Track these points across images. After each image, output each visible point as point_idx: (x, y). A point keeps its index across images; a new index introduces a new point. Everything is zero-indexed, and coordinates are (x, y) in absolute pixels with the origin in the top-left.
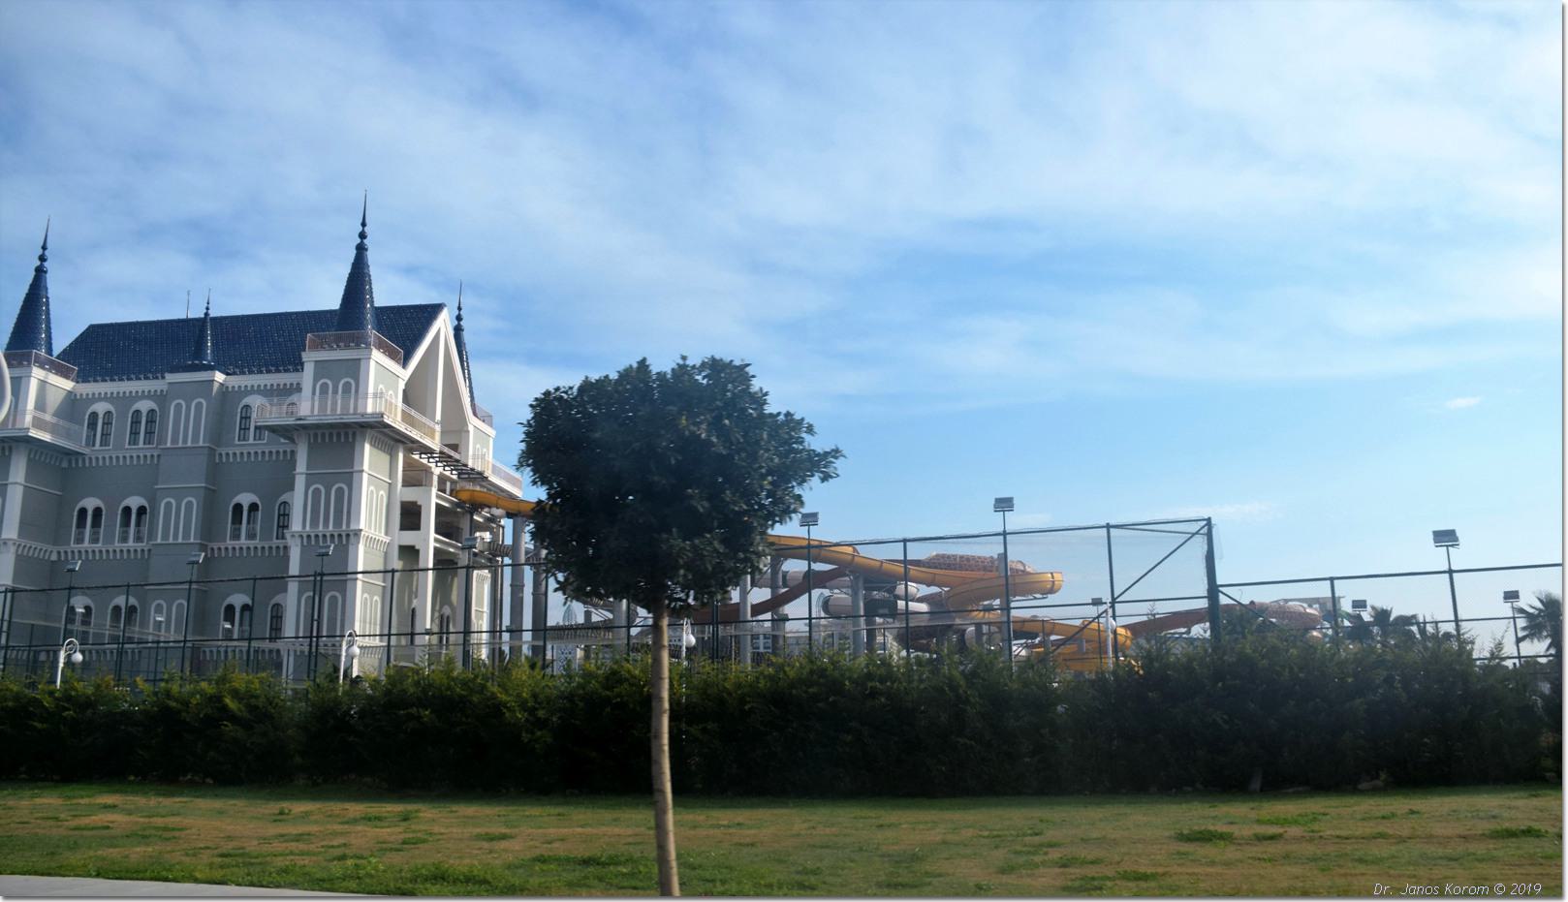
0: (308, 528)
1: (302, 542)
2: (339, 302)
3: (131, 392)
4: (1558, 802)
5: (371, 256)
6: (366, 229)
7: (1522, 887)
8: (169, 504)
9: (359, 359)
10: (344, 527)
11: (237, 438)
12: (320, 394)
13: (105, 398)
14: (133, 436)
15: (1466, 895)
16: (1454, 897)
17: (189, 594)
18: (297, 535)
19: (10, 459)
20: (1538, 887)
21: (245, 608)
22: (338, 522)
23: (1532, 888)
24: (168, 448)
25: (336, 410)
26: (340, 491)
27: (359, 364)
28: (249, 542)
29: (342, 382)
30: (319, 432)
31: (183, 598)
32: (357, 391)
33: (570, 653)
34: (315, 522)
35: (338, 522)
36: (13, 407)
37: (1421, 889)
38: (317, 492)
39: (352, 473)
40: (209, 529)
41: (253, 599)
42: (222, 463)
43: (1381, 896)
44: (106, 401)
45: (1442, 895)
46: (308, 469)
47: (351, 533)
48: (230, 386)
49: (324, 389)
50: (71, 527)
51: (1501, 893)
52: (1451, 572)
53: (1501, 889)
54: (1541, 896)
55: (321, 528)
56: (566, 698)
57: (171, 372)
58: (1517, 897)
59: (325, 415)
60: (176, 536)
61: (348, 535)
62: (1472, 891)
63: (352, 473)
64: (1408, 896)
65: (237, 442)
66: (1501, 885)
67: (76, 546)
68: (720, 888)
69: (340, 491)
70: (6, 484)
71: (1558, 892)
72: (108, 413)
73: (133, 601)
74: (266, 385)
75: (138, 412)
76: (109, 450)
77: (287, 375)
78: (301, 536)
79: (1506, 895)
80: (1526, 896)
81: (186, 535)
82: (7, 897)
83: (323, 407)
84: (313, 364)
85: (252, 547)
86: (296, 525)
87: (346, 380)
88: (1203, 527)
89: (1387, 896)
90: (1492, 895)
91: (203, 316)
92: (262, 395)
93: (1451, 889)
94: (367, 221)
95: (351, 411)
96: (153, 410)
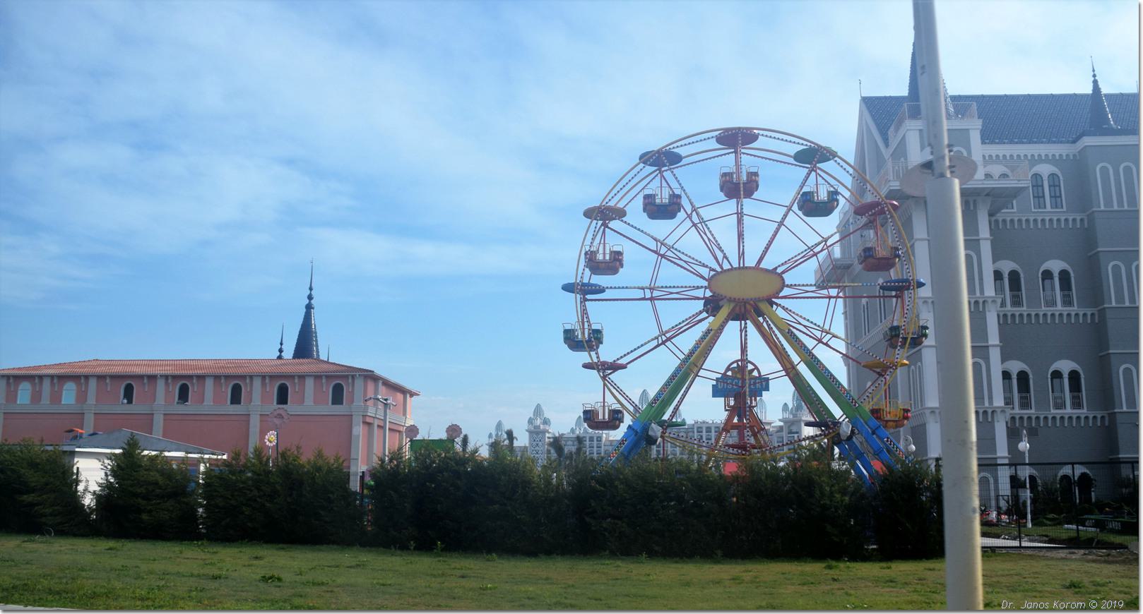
4: (1134, 537)
7: (1110, 604)
9: (968, 130)
14: (1041, 195)
15: (1069, 609)
16: (1059, 610)
19: (976, 212)
20: (1121, 603)
23: (1117, 604)
28: (1015, 309)
29: (1122, 167)
35: (922, 406)
37: (1036, 605)
39: (979, 240)
42: (1015, 229)
43: (1007, 610)
45: (1019, 609)
51: (1094, 607)
54: (1123, 609)
58: (1106, 610)
62: (1073, 606)
63: (979, 240)
64: (1026, 610)
65: (1033, 210)
66: (1094, 602)
68: (333, 606)
71: (1133, 604)
72: (1052, 175)
75: (1036, 176)
76: (1014, 213)
79: (1099, 609)
80: (1112, 609)
85: (1017, 314)
87: (1101, 165)
88: (785, 297)
89: (1011, 610)
90: (1087, 609)
91: (1088, 89)
96: (1053, 174)
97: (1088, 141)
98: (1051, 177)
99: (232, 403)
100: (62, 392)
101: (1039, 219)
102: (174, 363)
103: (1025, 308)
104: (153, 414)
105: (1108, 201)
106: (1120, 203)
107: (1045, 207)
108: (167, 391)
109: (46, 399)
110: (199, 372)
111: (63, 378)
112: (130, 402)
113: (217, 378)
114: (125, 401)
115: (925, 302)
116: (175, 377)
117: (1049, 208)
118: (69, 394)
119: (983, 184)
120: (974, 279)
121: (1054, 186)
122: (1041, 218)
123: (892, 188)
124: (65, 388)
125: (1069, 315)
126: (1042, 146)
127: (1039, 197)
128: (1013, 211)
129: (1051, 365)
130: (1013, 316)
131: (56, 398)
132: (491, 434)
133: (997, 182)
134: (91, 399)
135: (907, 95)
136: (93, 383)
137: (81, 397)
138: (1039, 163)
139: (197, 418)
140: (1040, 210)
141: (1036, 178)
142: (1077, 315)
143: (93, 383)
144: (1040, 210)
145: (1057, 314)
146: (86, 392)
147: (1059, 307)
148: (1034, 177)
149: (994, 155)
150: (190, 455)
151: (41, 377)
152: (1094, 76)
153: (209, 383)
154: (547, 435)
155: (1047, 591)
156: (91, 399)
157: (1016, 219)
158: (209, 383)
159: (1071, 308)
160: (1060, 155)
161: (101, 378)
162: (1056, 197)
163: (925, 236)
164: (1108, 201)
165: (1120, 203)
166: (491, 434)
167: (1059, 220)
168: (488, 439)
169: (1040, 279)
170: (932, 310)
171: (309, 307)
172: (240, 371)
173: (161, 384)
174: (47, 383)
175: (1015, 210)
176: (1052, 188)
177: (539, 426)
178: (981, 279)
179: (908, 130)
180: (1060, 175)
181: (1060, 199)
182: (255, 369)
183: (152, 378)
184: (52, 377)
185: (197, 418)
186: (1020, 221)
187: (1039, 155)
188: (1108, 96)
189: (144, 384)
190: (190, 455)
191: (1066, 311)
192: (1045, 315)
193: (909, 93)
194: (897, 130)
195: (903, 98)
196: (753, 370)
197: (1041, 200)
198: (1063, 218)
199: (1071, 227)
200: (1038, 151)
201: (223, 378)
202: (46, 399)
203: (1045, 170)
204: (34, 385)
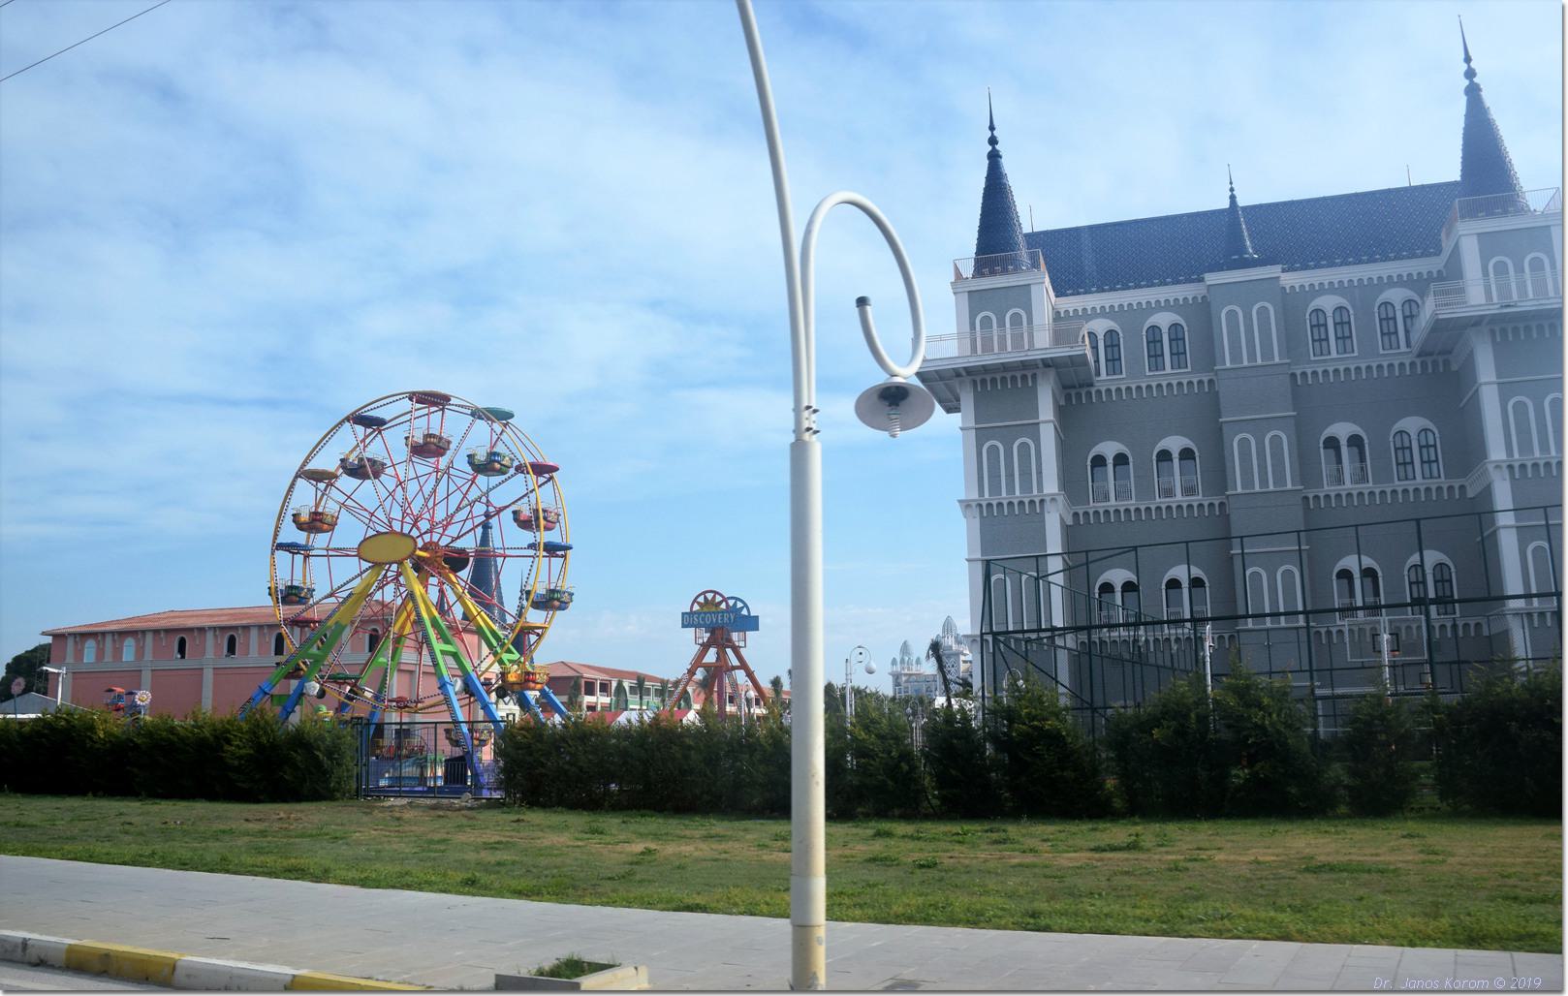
0: (987, 496)
1: (981, 512)
2: (1459, 167)
3: (1331, 283)
5: (1007, 164)
6: (1472, 65)
8: (1244, 443)
10: (1035, 492)
11: (1381, 348)
12: (1011, 325)
13: (1167, 306)
14: (1159, 353)
17: (1300, 554)
18: (974, 504)
20: (1538, 981)
21: (1129, 587)
22: (1026, 486)
23: (1532, 981)
24: (1277, 365)
25: (1526, 293)
26: (1024, 447)
27: (1550, 233)
30: (1008, 375)
31: (1542, 539)
32: (1030, 321)
33: (953, 666)
34: (995, 489)
35: (1026, 486)
36: (1560, 279)
38: (993, 450)
40: (1306, 471)
41: (1138, 576)
44: (1105, 317)
46: (1499, 376)
47: (1048, 499)
48: (1287, 287)
49: (1501, 270)
50: (1320, 463)
52: (1087, 564)
53: (1501, 983)
55: (1537, 454)
56: (579, 738)
57: (1211, 271)
59: (1548, 299)
60: (1264, 482)
61: (1042, 501)
67: (1163, 500)
69: (1024, 447)
70: (1038, 423)
72: (1175, 326)
73: (1196, 572)
74: (1176, 300)
75: (1154, 328)
77: (1138, 291)
78: (980, 505)
81: (1280, 479)
82: (6, 991)
83: (1504, 290)
84: (1475, 239)
86: (1496, 452)
91: (1225, 204)
92: (1405, 287)
93: (1452, 983)
94: (1471, 54)
95: (1026, 347)
96: (1111, 331)
97: (1212, 278)
98: (1108, 335)
99: (276, 654)
100: (122, 650)
101: (1320, 371)
102: (221, 613)
103: (1133, 502)
104: (141, 671)
105: (1236, 357)
106: (1252, 356)
107: (1329, 353)
108: (260, 645)
109: (108, 657)
110: (244, 622)
111: (123, 634)
112: (183, 657)
113: (260, 627)
114: (179, 656)
115: (1497, 467)
116: (223, 629)
117: (1168, 370)
118: (129, 651)
119: (1027, 356)
120: (1013, 475)
121: (1112, 346)
122: (1323, 369)
123: (1441, 317)
124: (86, 645)
125: (1190, 506)
126: (1178, 288)
127: (1156, 357)
128: (1352, 355)
129: (1166, 572)
130: (1428, 490)
131: (118, 653)
132: (894, 659)
133: (1009, 356)
134: (148, 656)
135: (1459, 179)
136: (149, 637)
137: (140, 652)
138: (1321, 295)
139: (245, 671)
140: (1179, 371)
141: (1153, 330)
142: (1201, 506)
143: (149, 637)
144: (1179, 371)
145: (1112, 510)
146: (143, 647)
147: (1179, 497)
148: (1173, 328)
149: (1153, 302)
150: (8, 716)
151: (104, 634)
152: (1232, 190)
153: (254, 633)
154: (962, 658)
155: (1501, 837)
156: (148, 656)
157: (1123, 388)
158: (254, 633)
159: (1339, 487)
160: (1148, 302)
161: (156, 632)
162: (1178, 354)
163: (1494, 379)
164: (1236, 357)
165: (1252, 356)
166: (894, 659)
167: (1391, 366)
168: (890, 666)
169: (1089, 468)
170: (1507, 477)
171: (1473, 92)
172: (191, 623)
173: (210, 635)
174: (109, 639)
175: (1124, 376)
176: (1174, 343)
177: (951, 647)
178: (1040, 473)
179: (1460, 236)
180: (1350, 308)
181: (1161, 358)
182: (206, 623)
183: (202, 630)
184: (113, 633)
185: (245, 671)
186: (1129, 389)
187: (1158, 302)
188: (1244, 209)
189: (161, 639)
190: (8, 716)
191: (1186, 501)
192: (1158, 508)
193: (1463, 176)
194: (1448, 235)
195: (1455, 184)
196: (699, 603)
197: (1324, 344)
198: (1396, 363)
199: (1353, 378)
200: (1386, 271)
201: (196, 631)
202: (108, 657)
203: (1164, 320)
204: (137, 641)
